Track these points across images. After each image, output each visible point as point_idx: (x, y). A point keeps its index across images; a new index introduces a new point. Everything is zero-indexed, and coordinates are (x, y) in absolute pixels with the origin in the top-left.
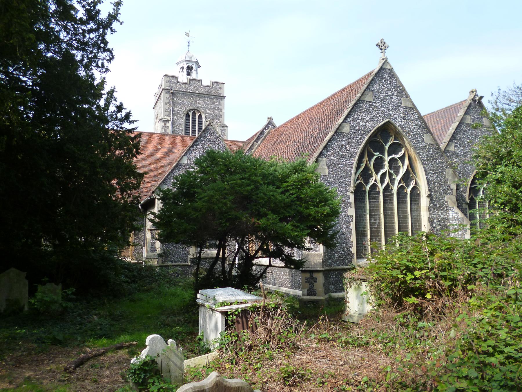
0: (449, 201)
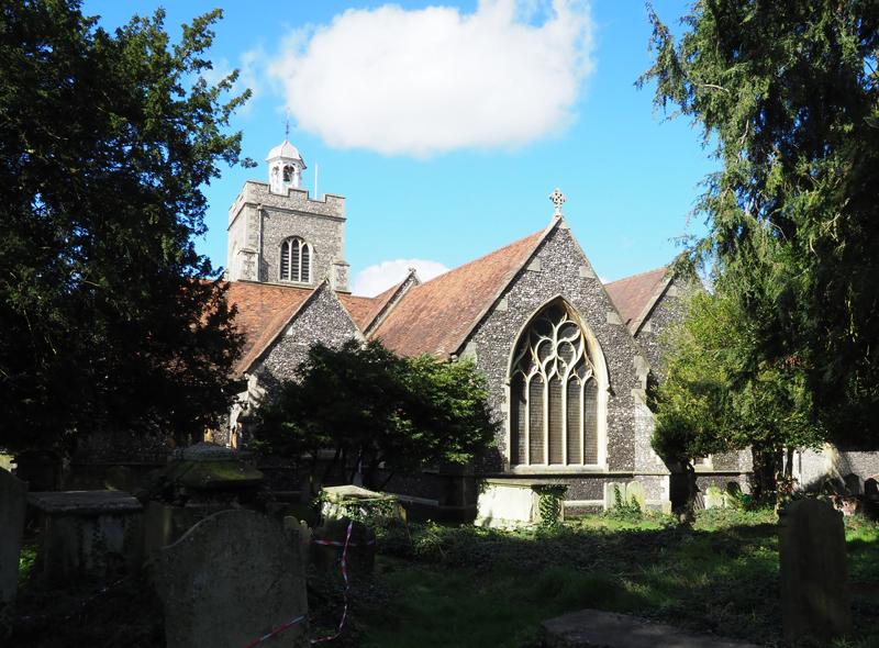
0: (636, 396)
